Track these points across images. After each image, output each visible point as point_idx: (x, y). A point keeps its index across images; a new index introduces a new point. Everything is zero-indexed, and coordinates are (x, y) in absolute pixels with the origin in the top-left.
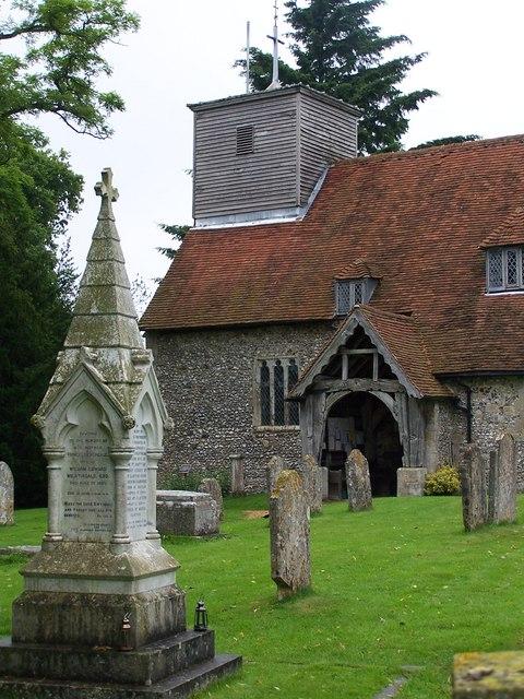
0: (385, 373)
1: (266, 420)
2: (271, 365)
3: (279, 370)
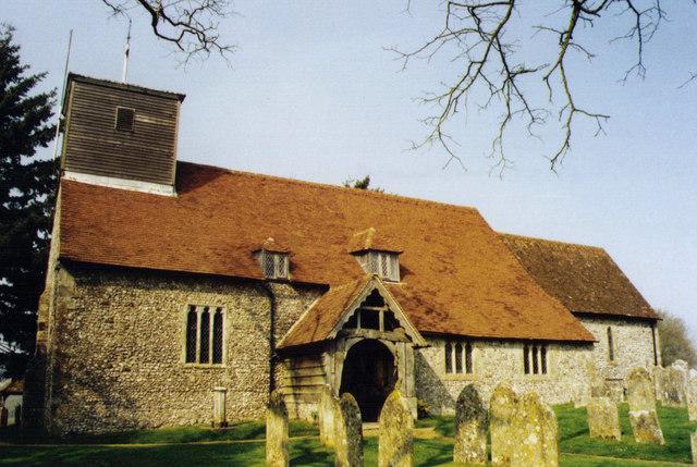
0: (392, 323)
1: (190, 358)
2: (199, 312)
3: (206, 316)
